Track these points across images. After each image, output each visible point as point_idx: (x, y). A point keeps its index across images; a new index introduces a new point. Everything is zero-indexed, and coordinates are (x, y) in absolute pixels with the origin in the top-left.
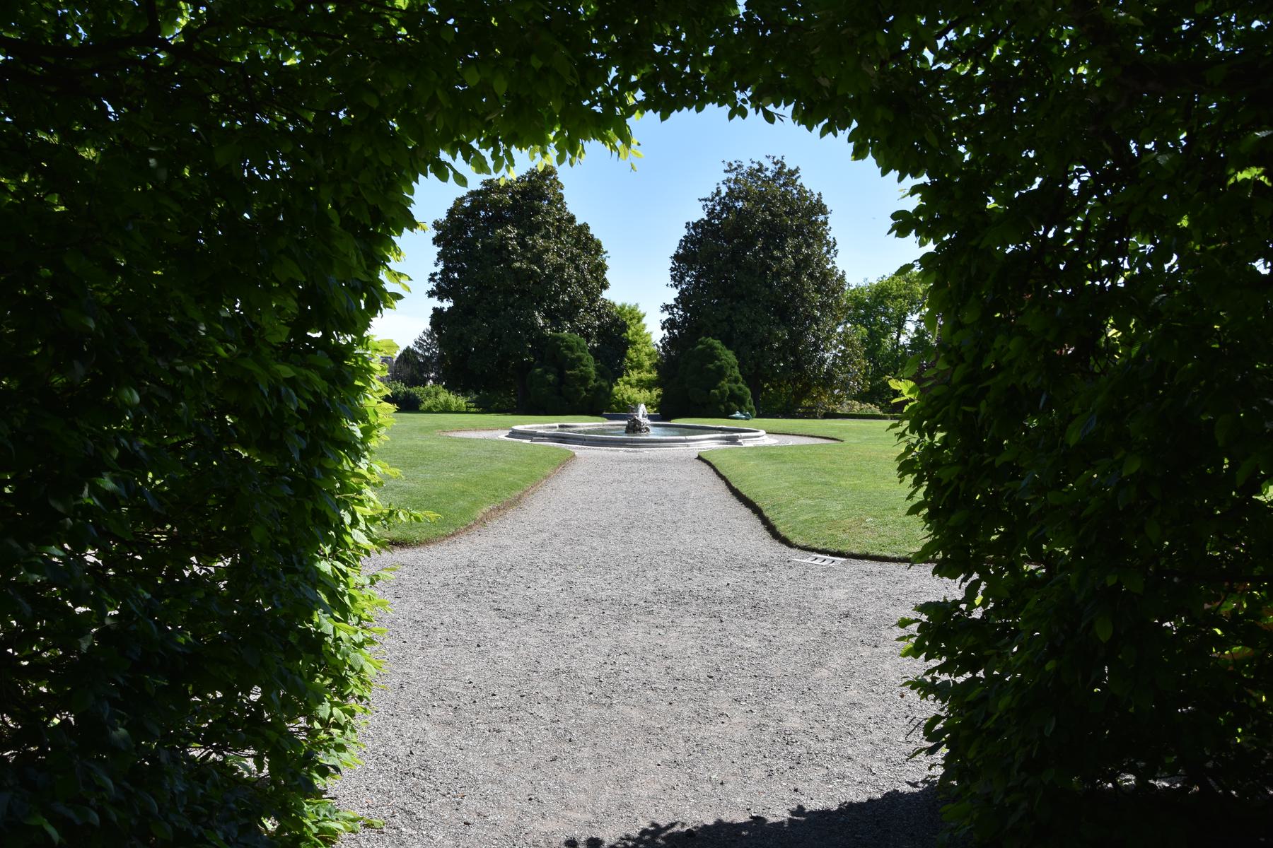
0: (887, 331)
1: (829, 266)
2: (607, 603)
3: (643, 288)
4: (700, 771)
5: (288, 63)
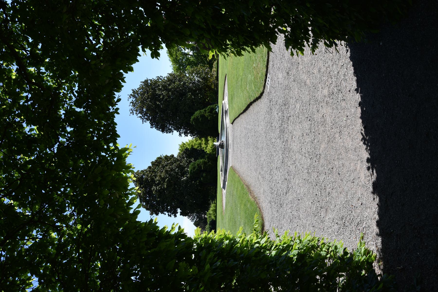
0: (188, 59)
1: (166, 79)
2: (284, 155)
3: (173, 143)
4: (343, 124)
5: (100, 266)
